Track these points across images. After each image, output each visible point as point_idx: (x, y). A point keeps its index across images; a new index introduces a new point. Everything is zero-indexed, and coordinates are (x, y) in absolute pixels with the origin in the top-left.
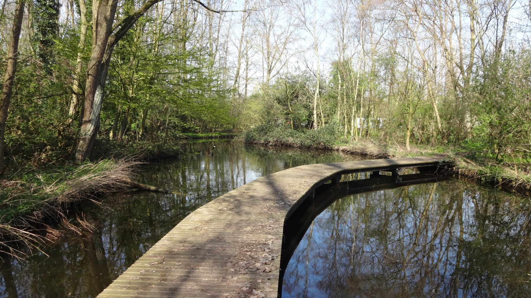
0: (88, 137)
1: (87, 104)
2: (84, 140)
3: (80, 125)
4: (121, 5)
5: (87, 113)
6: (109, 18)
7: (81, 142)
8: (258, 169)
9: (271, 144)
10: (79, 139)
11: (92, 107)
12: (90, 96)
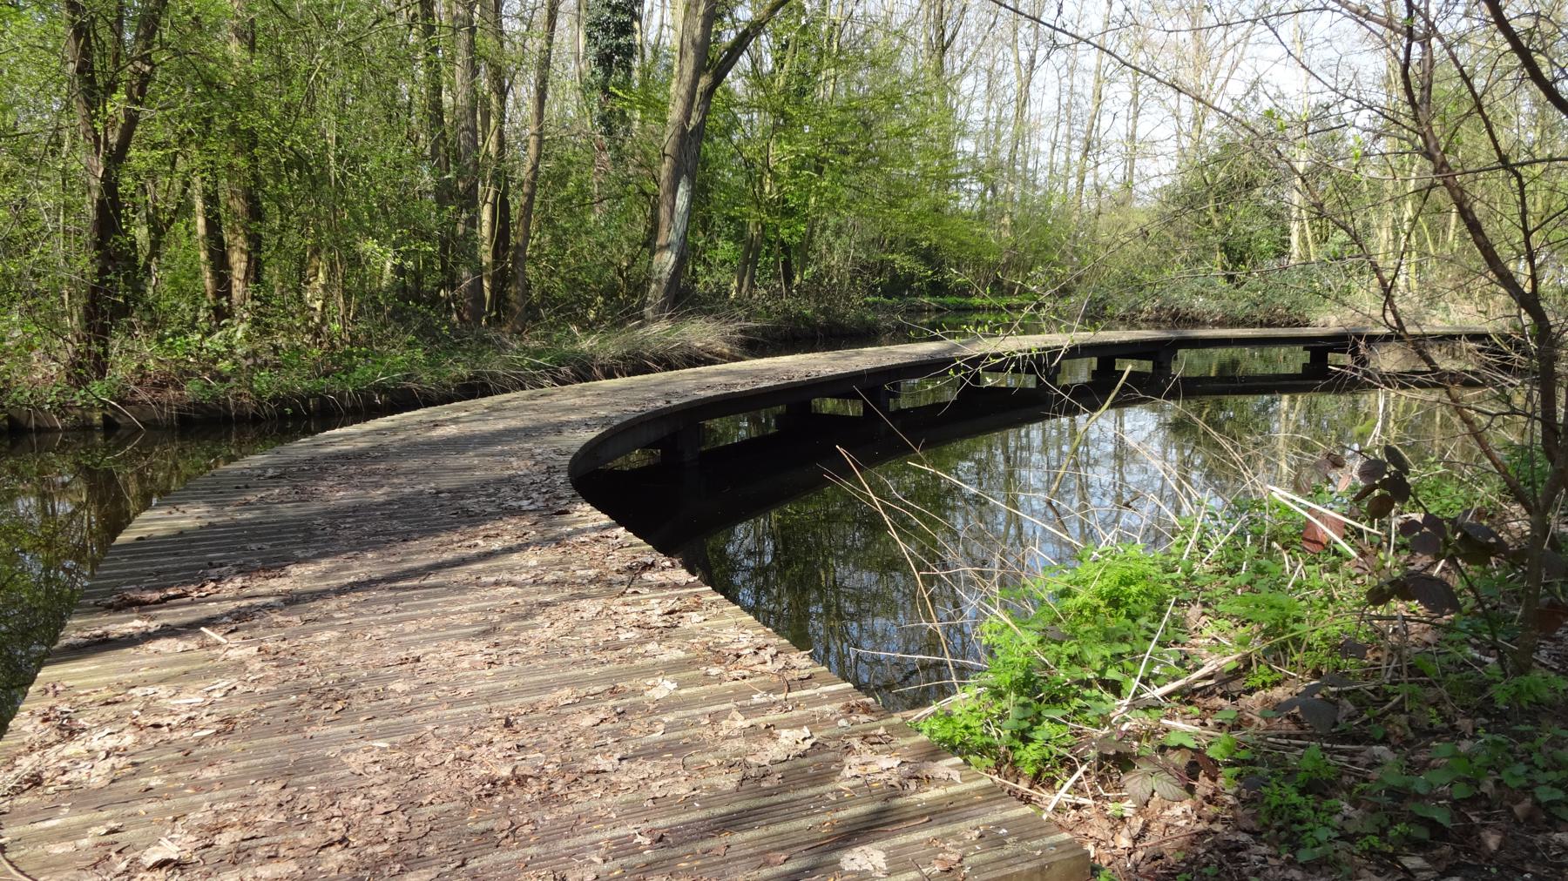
0: (665, 276)
1: (664, 213)
2: (659, 282)
3: (652, 254)
4: (270, 645)
5: (663, 230)
6: (698, 40)
7: (654, 286)
8: (1274, 412)
9: (1144, 316)
10: (649, 280)
11: (672, 219)
12: (669, 197)
